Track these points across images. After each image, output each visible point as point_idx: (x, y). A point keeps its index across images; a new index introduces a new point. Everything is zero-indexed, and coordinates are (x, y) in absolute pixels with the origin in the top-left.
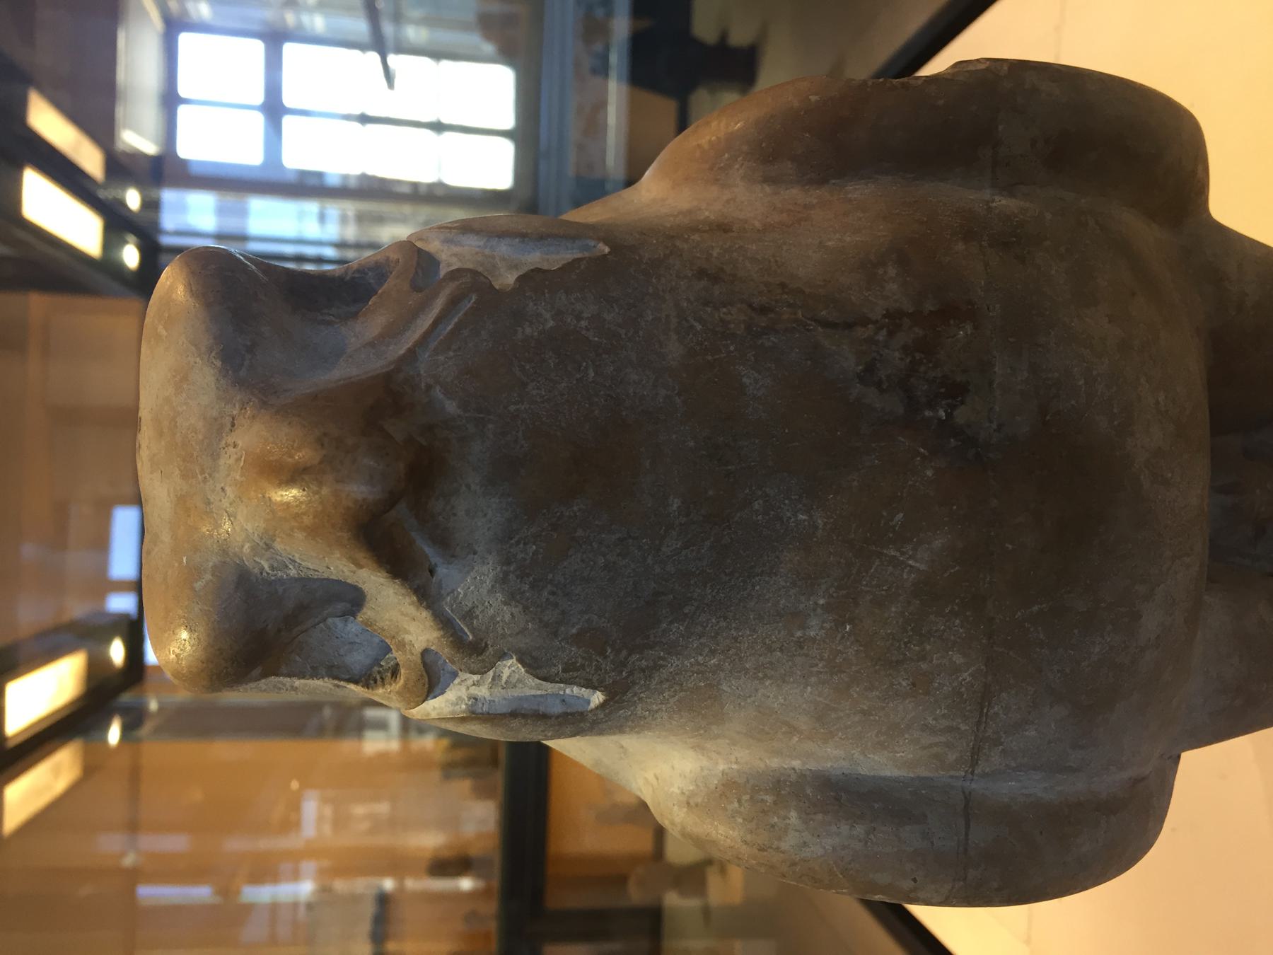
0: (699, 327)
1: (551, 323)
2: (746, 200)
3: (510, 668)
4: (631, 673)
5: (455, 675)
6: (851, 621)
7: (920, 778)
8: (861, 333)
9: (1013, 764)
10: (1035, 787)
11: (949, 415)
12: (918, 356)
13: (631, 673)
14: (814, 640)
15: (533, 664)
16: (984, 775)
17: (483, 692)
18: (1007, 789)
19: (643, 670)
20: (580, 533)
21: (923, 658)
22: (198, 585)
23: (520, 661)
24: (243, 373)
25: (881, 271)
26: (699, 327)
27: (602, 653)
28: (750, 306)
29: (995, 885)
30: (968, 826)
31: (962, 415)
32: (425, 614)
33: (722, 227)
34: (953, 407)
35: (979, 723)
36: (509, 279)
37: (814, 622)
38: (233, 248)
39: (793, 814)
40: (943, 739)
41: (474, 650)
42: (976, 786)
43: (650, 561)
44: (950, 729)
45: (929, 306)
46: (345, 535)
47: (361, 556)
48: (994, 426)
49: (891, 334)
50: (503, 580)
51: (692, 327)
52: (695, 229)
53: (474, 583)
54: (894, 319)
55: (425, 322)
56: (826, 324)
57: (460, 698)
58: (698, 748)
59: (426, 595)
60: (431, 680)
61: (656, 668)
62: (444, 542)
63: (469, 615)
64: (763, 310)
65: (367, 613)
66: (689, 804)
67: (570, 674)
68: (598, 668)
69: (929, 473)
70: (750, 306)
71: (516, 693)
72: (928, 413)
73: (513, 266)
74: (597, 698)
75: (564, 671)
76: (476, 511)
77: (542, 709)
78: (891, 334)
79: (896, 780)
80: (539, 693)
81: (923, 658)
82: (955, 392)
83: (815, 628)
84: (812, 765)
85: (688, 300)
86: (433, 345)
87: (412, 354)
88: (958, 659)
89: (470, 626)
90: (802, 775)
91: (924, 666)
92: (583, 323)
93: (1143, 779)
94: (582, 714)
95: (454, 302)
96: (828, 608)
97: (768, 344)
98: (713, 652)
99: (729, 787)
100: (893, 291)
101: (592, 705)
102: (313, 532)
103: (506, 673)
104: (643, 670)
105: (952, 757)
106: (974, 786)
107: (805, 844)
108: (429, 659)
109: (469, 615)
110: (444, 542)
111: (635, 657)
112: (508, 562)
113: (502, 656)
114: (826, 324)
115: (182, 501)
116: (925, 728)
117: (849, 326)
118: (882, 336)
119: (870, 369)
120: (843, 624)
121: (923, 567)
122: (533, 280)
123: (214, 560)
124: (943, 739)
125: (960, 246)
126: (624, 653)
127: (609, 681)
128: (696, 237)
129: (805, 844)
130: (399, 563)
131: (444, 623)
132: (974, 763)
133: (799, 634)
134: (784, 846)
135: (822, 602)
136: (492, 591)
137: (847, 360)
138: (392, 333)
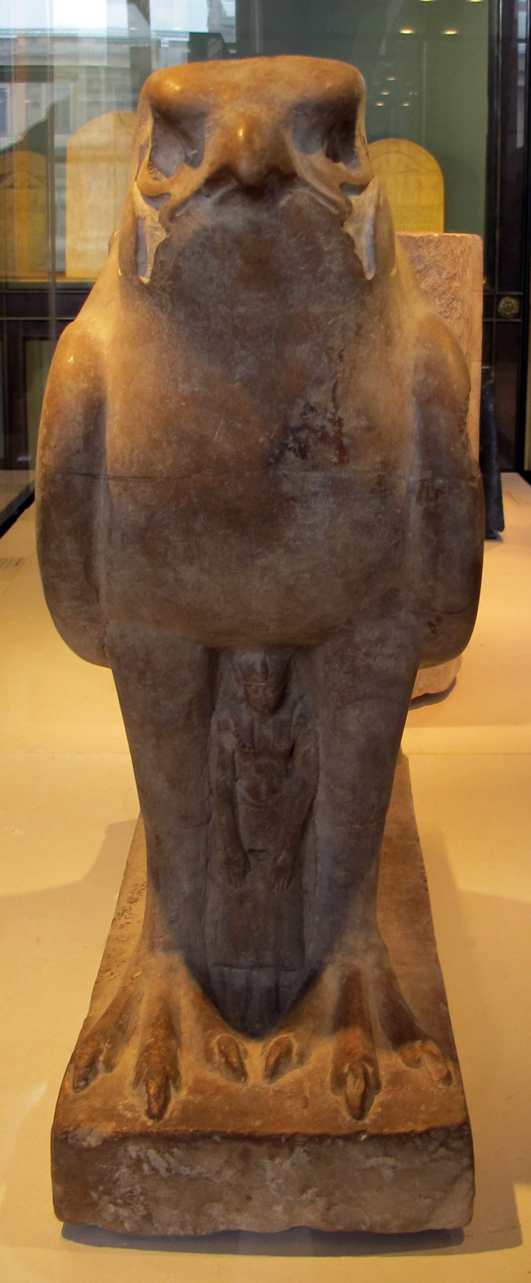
0: (330, 323)
1: (326, 249)
2: (407, 355)
3: (161, 235)
4: (159, 295)
5: (157, 209)
6: (187, 405)
7: (105, 452)
8: (330, 405)
9: (114, 501)
10: (101, 517)
11: (290, 449)
12: (320, 433)
13: (159, 295)
14: (177, 387)
15: (164, 246)
16: (108, 485)
17: (148, 222)
18: (101, 500)
19: (160, 300)
21: (169, 443)
22: (200, 96)
23: (166, 239)
24: (294, 112)
25: (363, 417)
26: (330, 323)
27: (169, 279)
28: (342, 350)
29: (53, 490)
30: (82, 475)
31: (290, 455)
32: (188, 193)
33: (388, 341)
34: (294, 451)
35: (136, 477)
36: (350, 229)
37: (186, 386)
41: (171, 217)
42: (102, 482)
43: (215, 299)
44: (132, 463)
45: (346, 441)
46: (224, 160)
47: (215, 167)
48: (286, 472)
49: (330, 420)
50: (205, 229)
51: (329, 319)
52: (387, 327)
53: (205, 214)
54: (339, 423)
55: (324, 189)
56: (335, 388)
57: (144, 211)
59: (197, 193)
60: (153, 197)
61: (162, 307)
62: (222, 201)
63: (188, 214)
64: (341, 357)
65: (187, 168)
66: (84, 337)
67: (159, 264)
68: (162, 278)
69: (261, 440)
70: (342, 350)
71: (148, 238)
72: (291, 438)
73: (359, 232)
74: (146, 280)
76: (237, 216)
77: (140, 252)
78: (330, 420)
79: (104, 439)
80: (148, 251)
82: (302, 452)
83: (183, 387)
84: (109, 397)
85: (344, 318)
86: (313, 194)
87: (306, 184)
88: (169, 462)
89: (182, 215)
90: (104, 391)
91: (165, 445)
92: (327, 265)
93: (98, 600)
94: (137, 272)
95: (333, 203)
96: (193, 392)
97: (323, 358)
98: (169, 336)
99: (95, 356)
100: (352, 424)
101: (141, 278)
102: (225, 147)
103: (158, 233)
104: (160, 300)
106: (102, 481)
107: (71, 391)
108: (166, 196)
109: (188, 214)
111: (168, 296)
112: (213, 230)
113: (168, 230)
114: (335, 388)
115: (236, 87)
116: (132, 450)
117: (334, 399)
118: (329, 415)
119: (312, 409)
120: (185, 401)
121: (215, 439)
122: (349, 243)
123: (211, 102)
125: (378, 459)
126: (169, 290)
127: (155, 284)
128: (382, 327)
130: (212, 182)
131: (184, 203)
132: (114, 478)
133: (180, 379)
135: (196, 389)
137: (318, 396)
138: (318, 174)
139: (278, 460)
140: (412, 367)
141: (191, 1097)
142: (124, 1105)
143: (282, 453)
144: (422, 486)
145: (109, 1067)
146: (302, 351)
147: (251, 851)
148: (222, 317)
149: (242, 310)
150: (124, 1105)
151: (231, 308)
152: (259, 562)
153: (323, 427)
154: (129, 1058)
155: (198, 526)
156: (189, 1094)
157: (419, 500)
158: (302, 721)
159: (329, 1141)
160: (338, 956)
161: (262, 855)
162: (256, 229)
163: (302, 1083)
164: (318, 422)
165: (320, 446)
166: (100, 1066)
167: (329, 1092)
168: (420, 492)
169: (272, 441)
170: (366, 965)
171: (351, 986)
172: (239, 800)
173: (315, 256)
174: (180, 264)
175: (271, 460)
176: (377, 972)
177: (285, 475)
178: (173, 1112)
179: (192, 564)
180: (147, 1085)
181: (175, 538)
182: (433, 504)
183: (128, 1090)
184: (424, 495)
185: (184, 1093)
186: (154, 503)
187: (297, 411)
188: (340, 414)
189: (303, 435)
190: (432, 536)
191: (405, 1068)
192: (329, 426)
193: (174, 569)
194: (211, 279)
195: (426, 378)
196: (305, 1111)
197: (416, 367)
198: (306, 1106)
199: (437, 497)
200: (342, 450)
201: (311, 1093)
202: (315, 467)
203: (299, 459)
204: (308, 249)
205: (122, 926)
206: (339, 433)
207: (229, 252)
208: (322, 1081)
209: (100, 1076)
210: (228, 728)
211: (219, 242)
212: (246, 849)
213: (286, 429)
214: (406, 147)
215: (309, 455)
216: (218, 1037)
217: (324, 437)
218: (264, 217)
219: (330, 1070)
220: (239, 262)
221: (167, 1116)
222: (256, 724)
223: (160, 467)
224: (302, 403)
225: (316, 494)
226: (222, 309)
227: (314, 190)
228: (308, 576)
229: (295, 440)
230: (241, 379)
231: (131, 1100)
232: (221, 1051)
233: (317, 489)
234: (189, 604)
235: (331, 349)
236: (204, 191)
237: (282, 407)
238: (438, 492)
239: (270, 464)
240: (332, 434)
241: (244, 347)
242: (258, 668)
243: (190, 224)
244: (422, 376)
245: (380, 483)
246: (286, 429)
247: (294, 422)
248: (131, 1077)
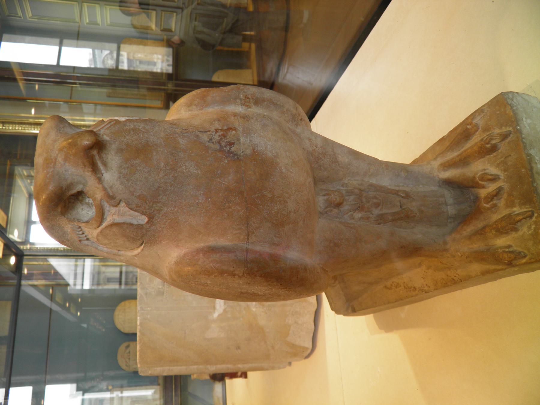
14: (201, 203)
20: (138, 168)
31: (233, 149)
35: (247, 227)
37: (200, 198)
38: (81, 375)
39: (201, 255)
40: (238, 232)
42: (250, 247)
43: (156, 178)
45: (225, 128)
49: (216, 133)
54: (216, 130)
56: (200, 132)
58: (177, 246)
62: (105, 164)
69: (226, 161)
75: (136, 207)
78: (216, 133)
81: (230, 208)
82: (232, 144)
84: (207, 244)
86: (105, 128)
87: (99, 130)
88: (239, 208)
91: (230, 210)
103: (122, 209)
105: (242, 237)
107: (205, 261)
110: (105, 164)
111: (154, 205)
114: (200, 132)
117: (206, 132)
118: (213, 134)
119: (211, 140)
124: (238, 232)
125: (233, 118)
126: (151, 203)
129: (205, 261)
132: (248, 239)
134: (199, 263)
136: (117, 180)
137: (205, 138)
139: (236, 155)
140: (190, 112)
141: (517, 205)
142: (528, 231)
143: (232, 153)
144: (244, 104)
145: (509, 246)
146: (183, 142)
147: (401, 207)
148: (166, 175)
149: (162, 164)
150: (528, 231)
151: (161, 170)
152: (284, 170)
153: (219, 136)
154: (501, 242)
155: (269, 195)
156: (515, 207)
157: (250, 107)
158: (345, 185)
159: (524, 140)
160: (435, 174)
161: (402, 203)
162: (120, 151)
163: (498, 164)
164: (217, 137)
165: (228, 137)
166: (511, 249)
167: (500, 151)
168: (247, 106)
169: (227, 157)
170: (436, 164)
171: (447, 166)
172: (381, 212)
173: (135, 131)
174: (138, 194)
175: (236, 157)
176: (438, 159)
177: (243, 152)
178: (527, 208)
179: (287, 202)
180: (518, 222)
181: (276, 208)
182: (251, 100)
183: (520, 233)
184: (247, 104)
185: (515, 209)
186: (259, 217)
187: (211, 145)
188: (213, 130)
189: (223, 144)
190: (265, 103)
191: (480, 129)
192: (218, 134)
193: (290, 212)
194: (146, 178)
195: (195, 105)
196: (512, 155)
197: (189, 110)
198: (510, 156)
199: (248, 98)
200: (229, 129)
201: (502, 157)
202: (238, 140)
203: (235, 146)
204: (132, 133)
205: (429, 287)
206: (222, 130)
207: (132, 166)
208: (495, 156)
209: (515, 248)
210: (352, 215)
211: (126, 171)
212: (400, 209)
213: (221, 150)
214: (117, 313)
215: (232, 141)
216: (485, 205)
217: (224, 135)
218: (114, 146)
219: (488, 157)
220: (138, 161)
221: (530, 209)
222: (349, 203)
223: (241, 213)
224: (207, 144)
225: (251, 141)
226: (162, 174)
227: (102, 128)
228: (287, 153)
229: (225, 147)
230: (197, 170)
231: (525, 229)
232: (491, 201)
233: (248, 140)
234: (304, 210)
235: (181, 132)
236: (99, 176)
237: (210, 151)
238: (246, 97)
239: (238, 158)
240: (222, 133)
241: (181, 167)
242: (326, 198)
243: (117, 187)
244: (194, 107)
245: (244, 118)
246: (221, 150)
247: (217, 147)
248: (514, 235)
